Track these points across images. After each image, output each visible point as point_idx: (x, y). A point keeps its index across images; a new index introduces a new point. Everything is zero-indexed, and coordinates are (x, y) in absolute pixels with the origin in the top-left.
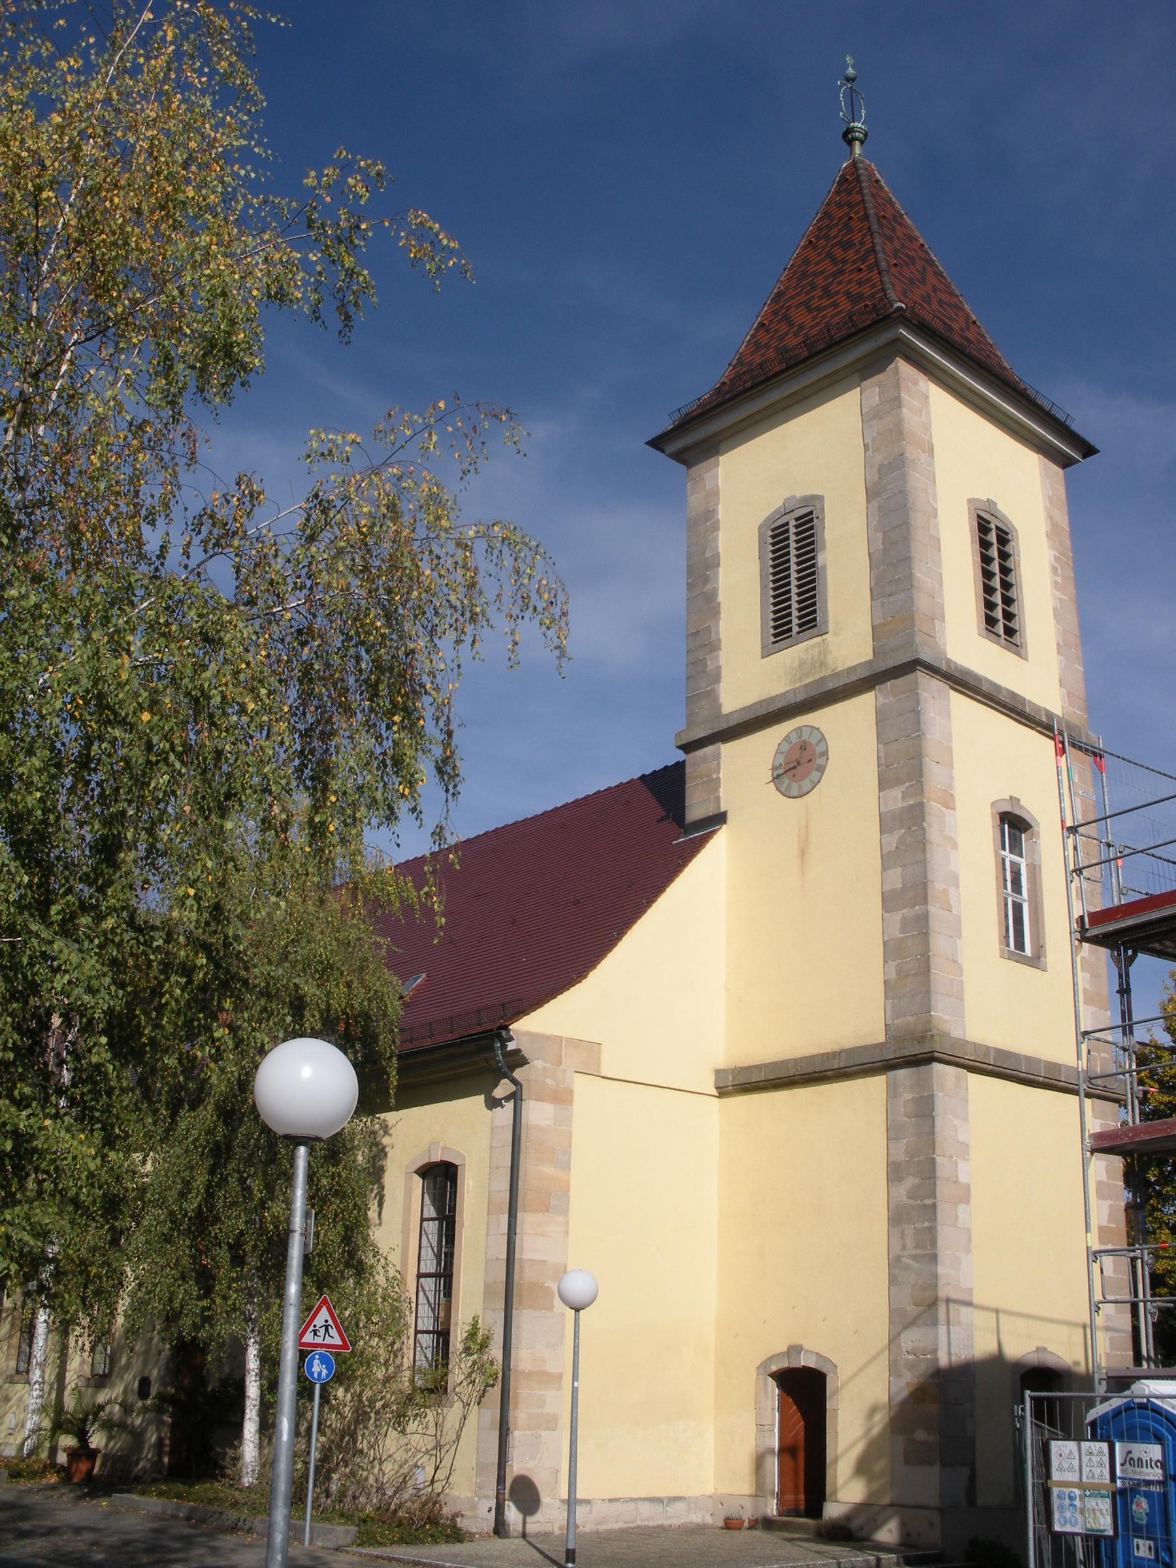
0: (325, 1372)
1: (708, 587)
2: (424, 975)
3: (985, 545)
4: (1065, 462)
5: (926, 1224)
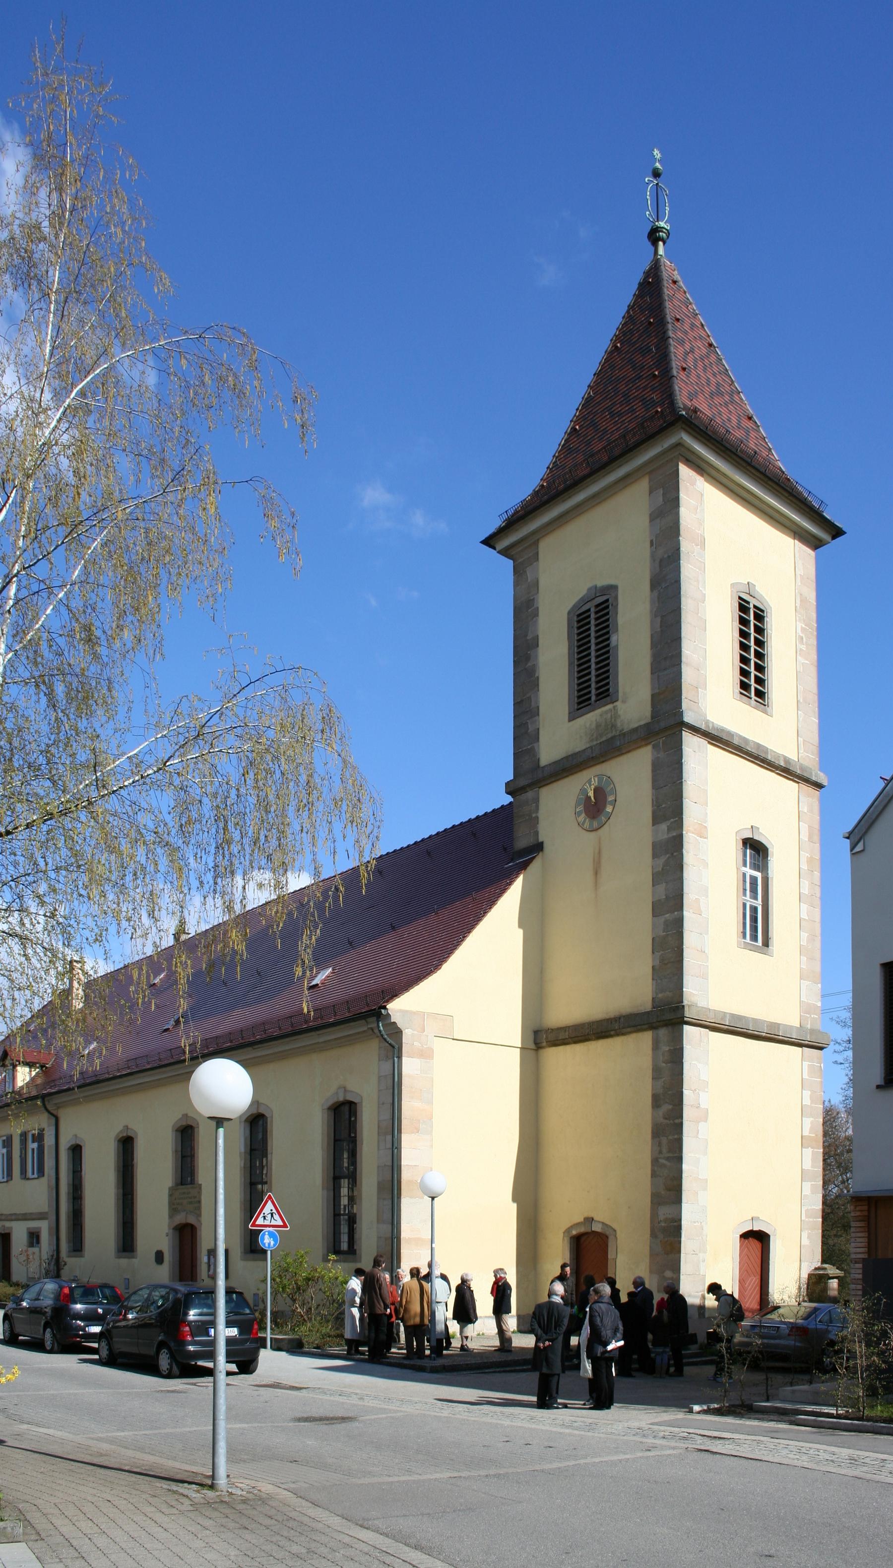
0: (272, 1243)
1: (529, 664)
2: (330, 970)
3: (743, 622)
4: (815, 544)
5: (676, 1137)
